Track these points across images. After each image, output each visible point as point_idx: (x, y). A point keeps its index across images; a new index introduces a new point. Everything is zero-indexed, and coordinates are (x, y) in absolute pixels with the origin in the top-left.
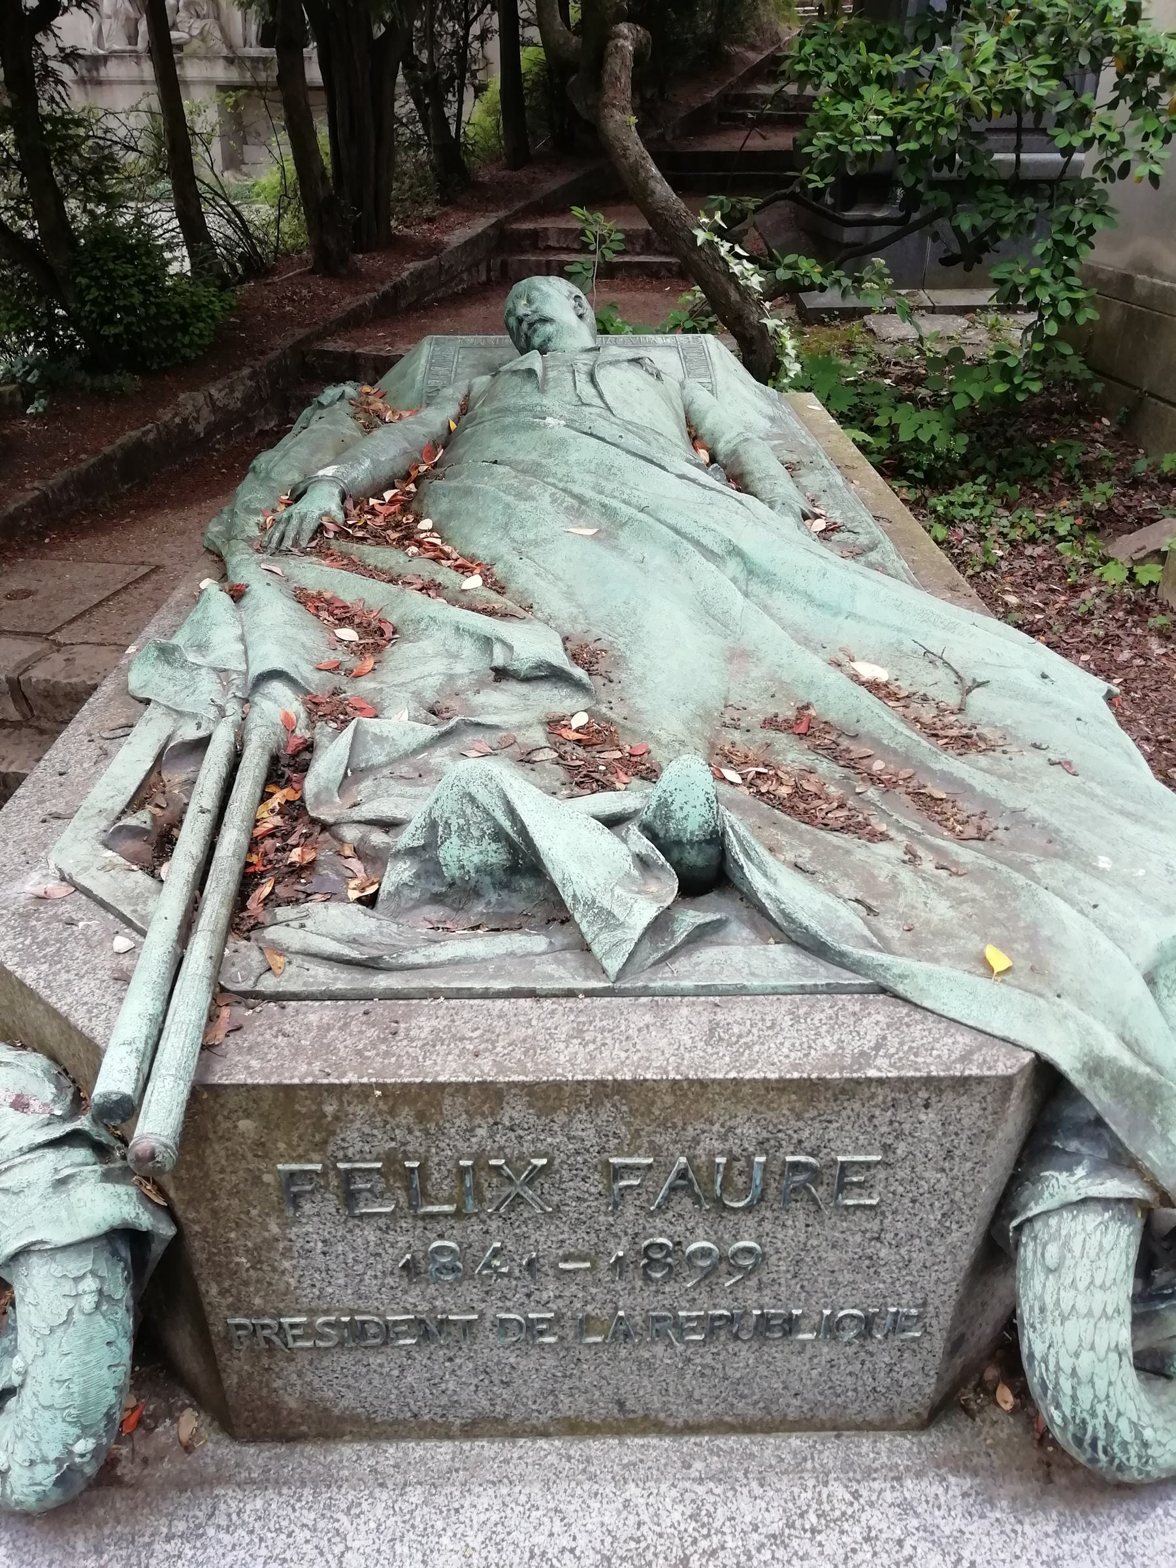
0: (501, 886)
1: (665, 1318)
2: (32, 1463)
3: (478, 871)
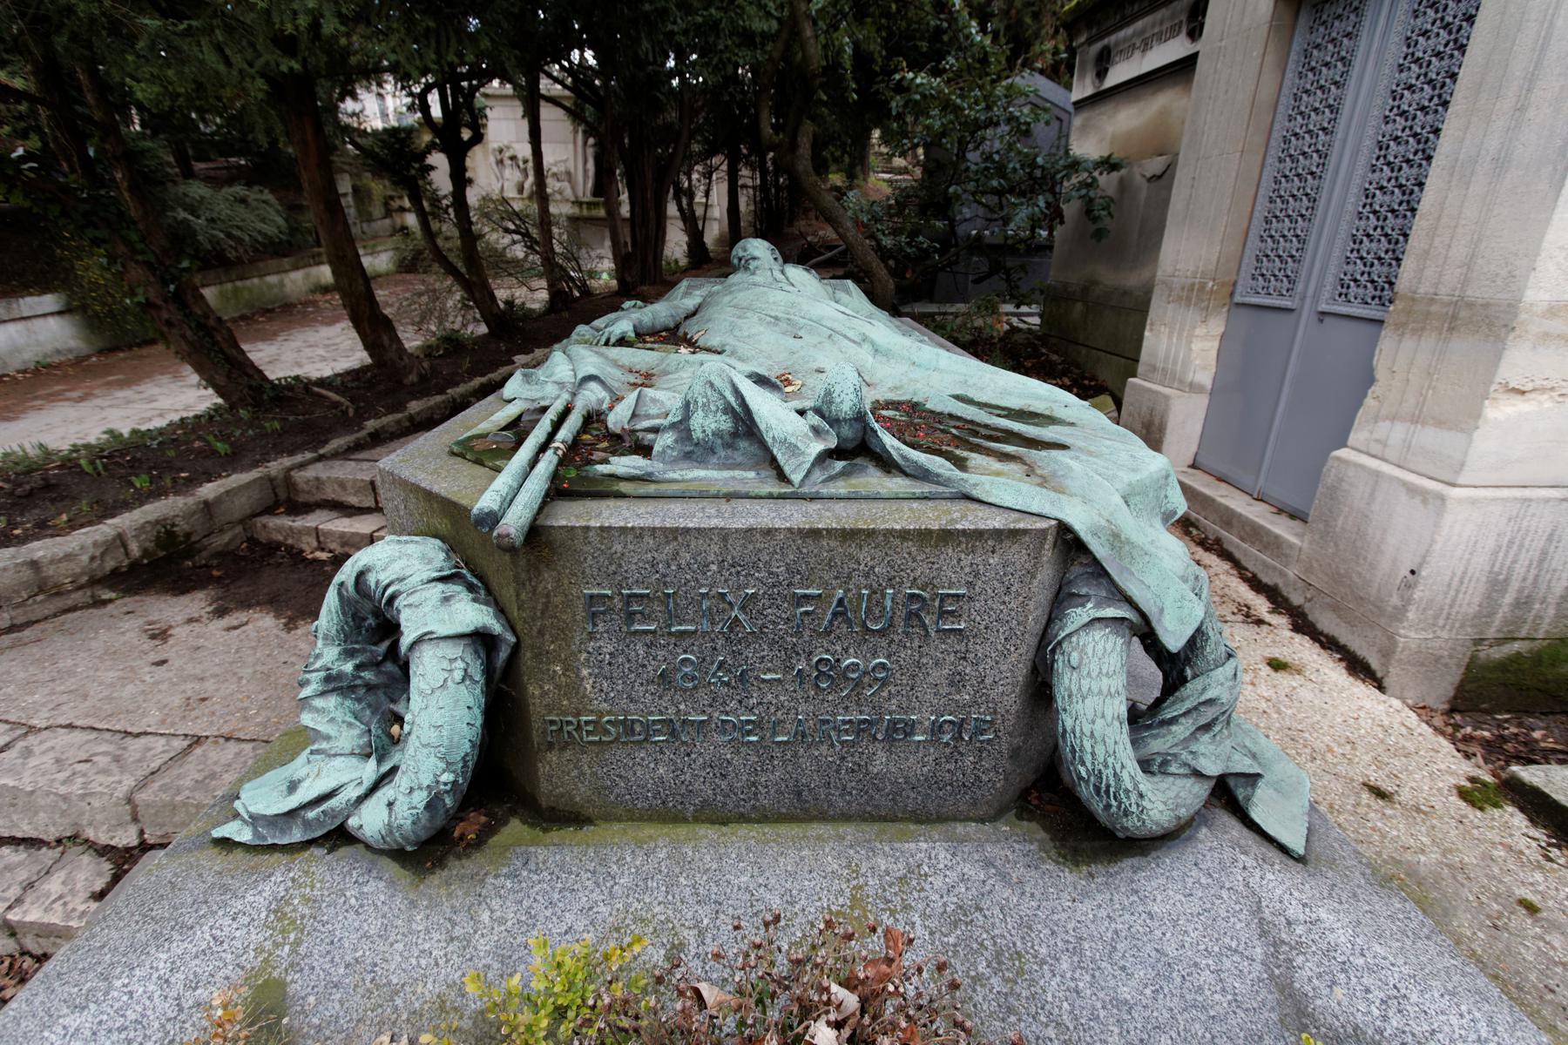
0: (727, 446)
1: (828, 721)
2: (412, 790)
3: (714, 434)
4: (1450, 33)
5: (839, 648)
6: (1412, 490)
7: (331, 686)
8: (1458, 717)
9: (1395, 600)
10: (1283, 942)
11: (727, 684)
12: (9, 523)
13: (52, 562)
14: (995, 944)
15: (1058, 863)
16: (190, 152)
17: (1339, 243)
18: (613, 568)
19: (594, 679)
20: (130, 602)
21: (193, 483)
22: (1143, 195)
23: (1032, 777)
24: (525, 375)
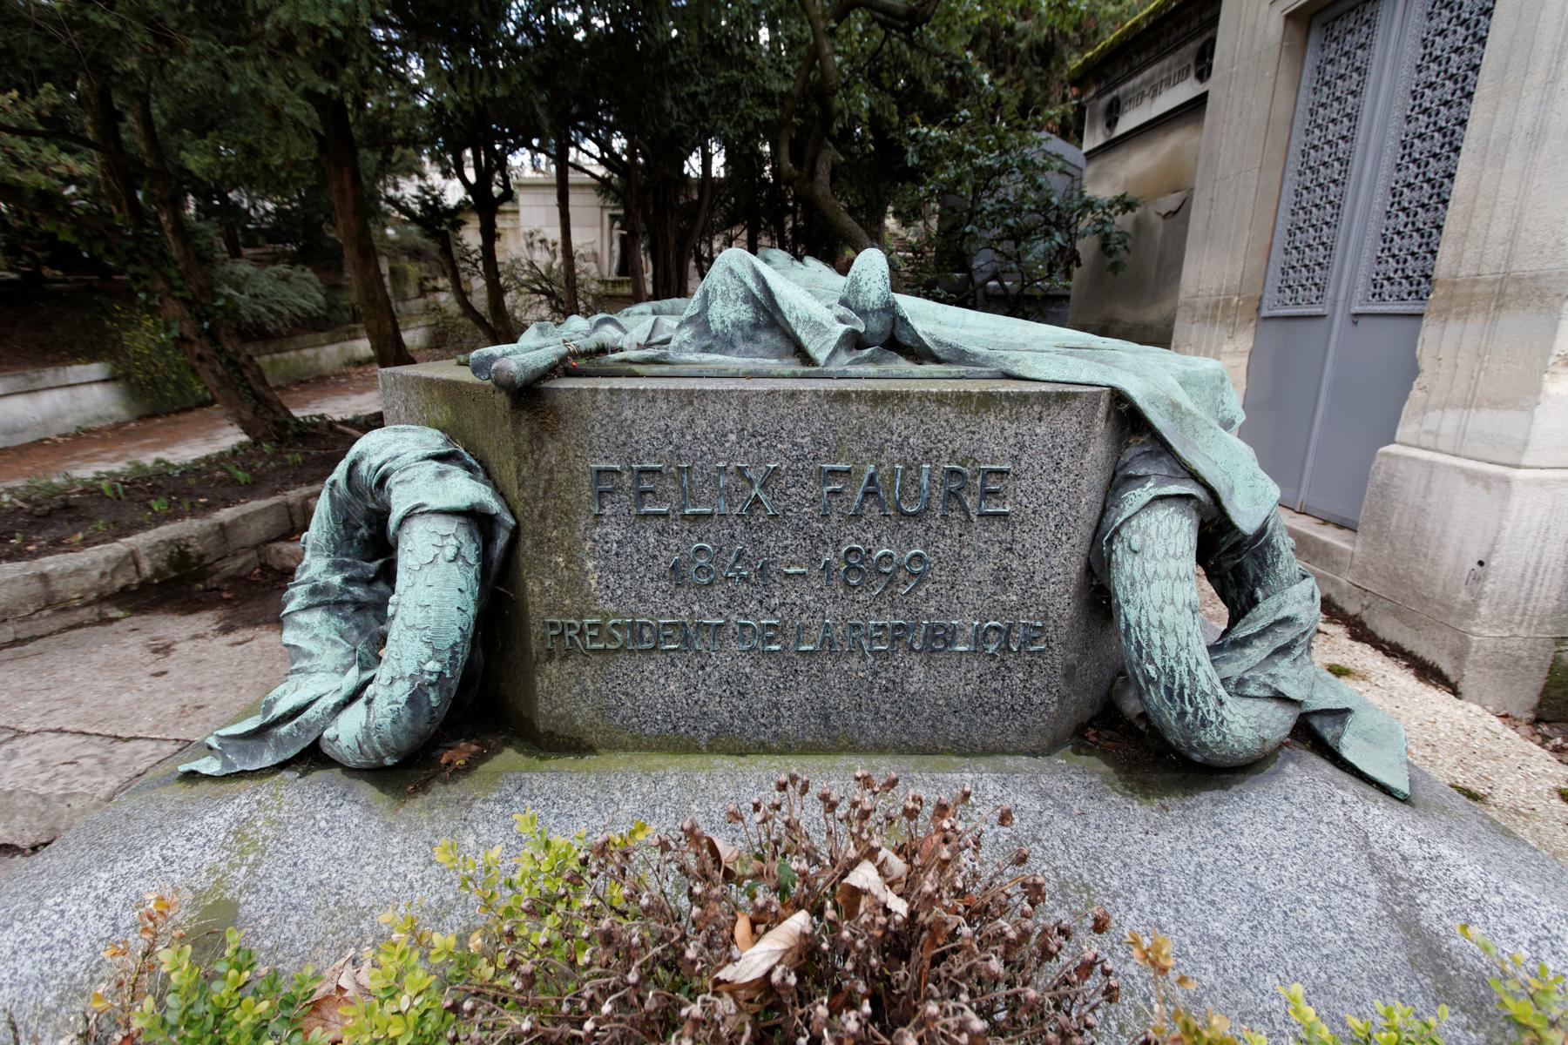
0: (749, 339)
1: (858, 627)
2: (393, 680)
3: (733, 325)
4: (1468, 28)
5: (870, 536)
6: (1472, 477)
7: (317, 600)
8: (1545, 728)
9: (1463, 596)
10: (1401, 878)
11: (745, 579)
12: (24, 540)
13: (62, 576)
14: (1058, 875)
15: (1124, 795)
16: (240, 239)
17: (1368, 243)
18: (623, 438)
19: (600, 572)
20: (136, 621)
21: (211, 507)
22: (1160, 232)
23: (1089, 713)
24: (540, 328)
